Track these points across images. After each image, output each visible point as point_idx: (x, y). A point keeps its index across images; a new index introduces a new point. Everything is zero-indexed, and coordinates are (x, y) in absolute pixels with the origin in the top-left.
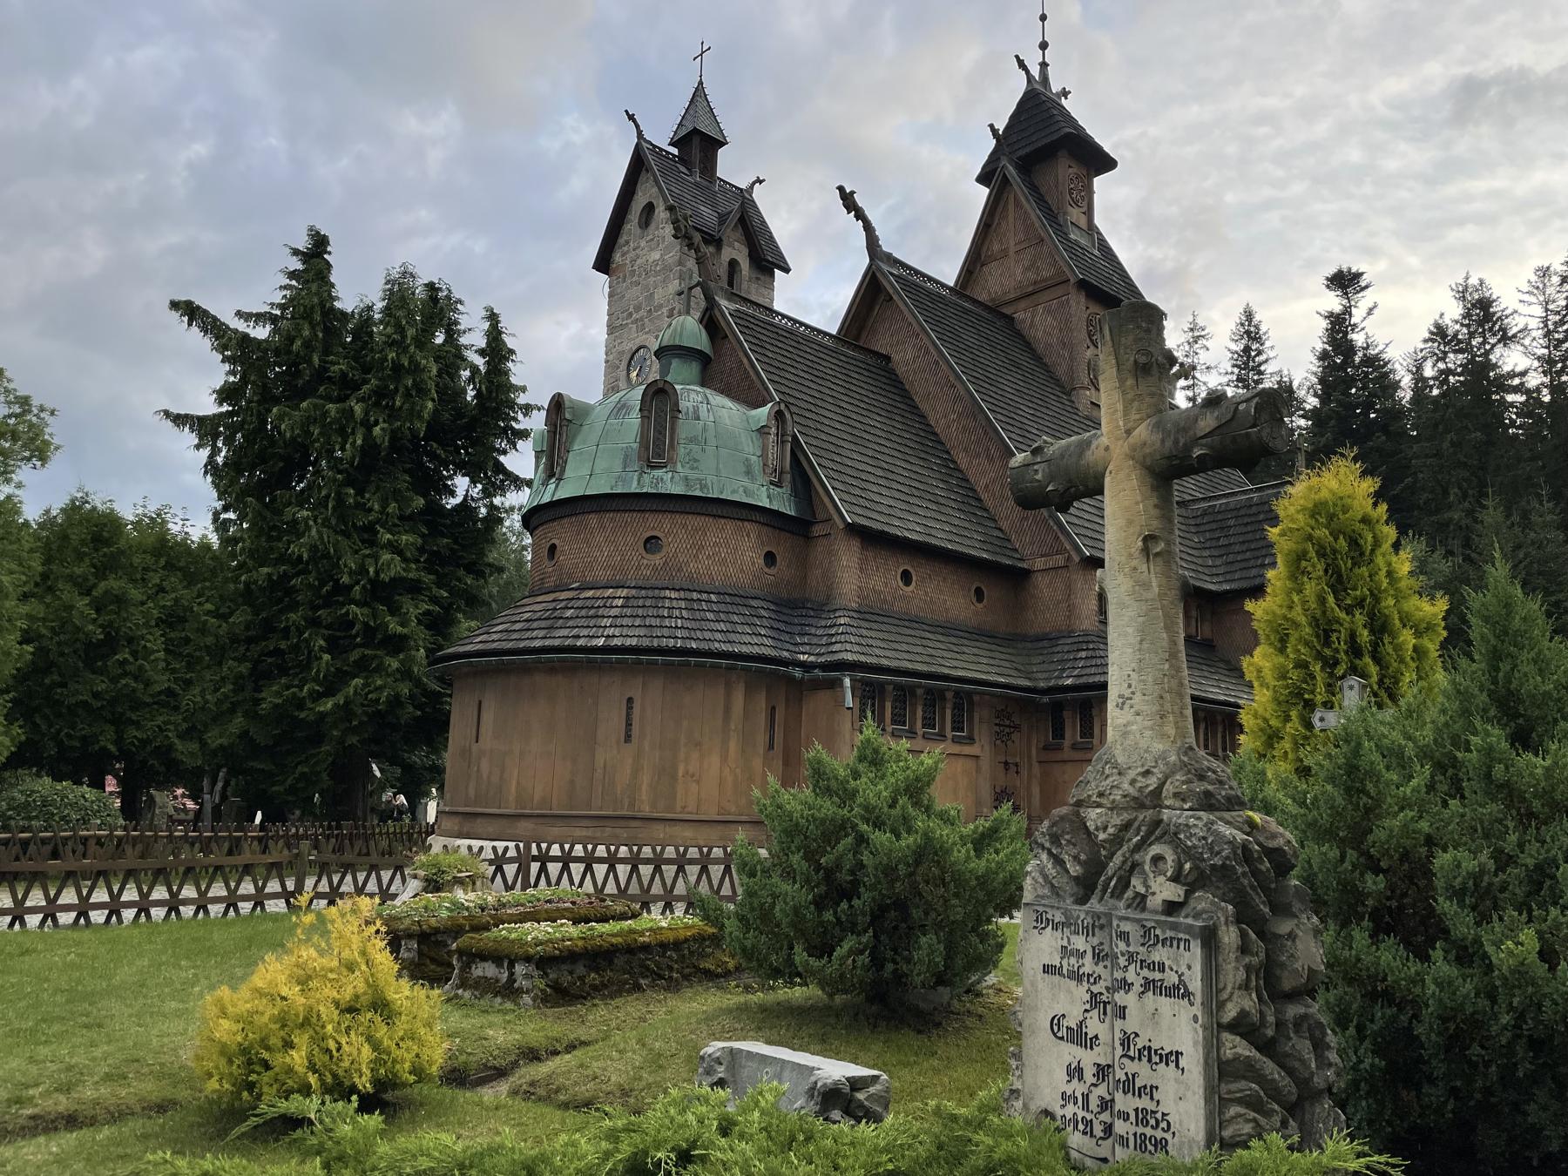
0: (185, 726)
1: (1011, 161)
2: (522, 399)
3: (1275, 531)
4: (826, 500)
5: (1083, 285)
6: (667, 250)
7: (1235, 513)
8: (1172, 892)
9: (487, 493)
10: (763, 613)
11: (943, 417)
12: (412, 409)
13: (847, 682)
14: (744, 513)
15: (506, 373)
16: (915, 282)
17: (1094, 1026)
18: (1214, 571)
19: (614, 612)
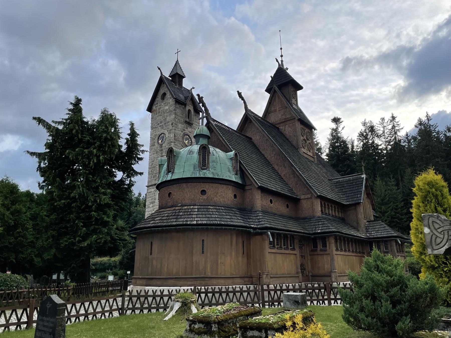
0: (37, 253)
1: (276, 86)
2: (142, 149)
3: (414, 189)
4: (251, 179)
7: (346, 183)
9: (128, 176)
11: (269, 154)
12: (111, 151)
15: (137, 140)
18: (343, 199)
19: (195, 213)
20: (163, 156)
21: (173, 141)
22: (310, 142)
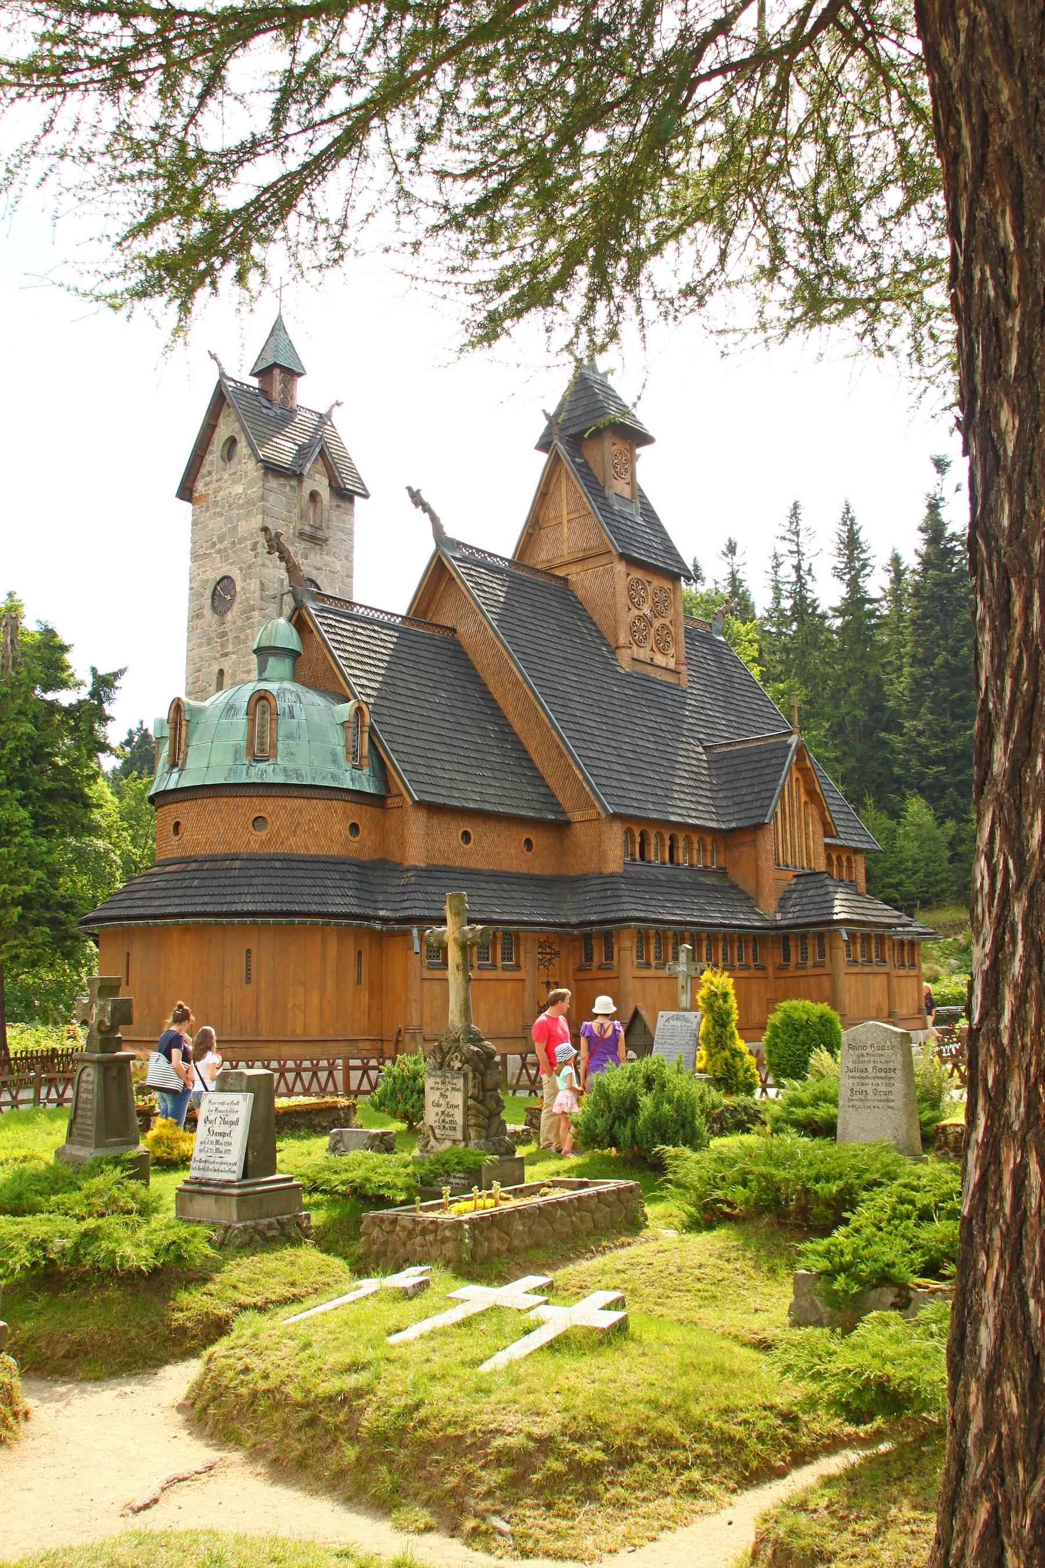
4: (398, 780)
5: (623, 557)
6: (250, 484)
8: (459, 1065)
10: (349, 876)
13: (415, 932)
14: (332, 794)
15: (71, 705)
16: (479, 560)
17: (442, 1101)
20: (226, 655)
21: (257, 603)
22: (666, 621)
